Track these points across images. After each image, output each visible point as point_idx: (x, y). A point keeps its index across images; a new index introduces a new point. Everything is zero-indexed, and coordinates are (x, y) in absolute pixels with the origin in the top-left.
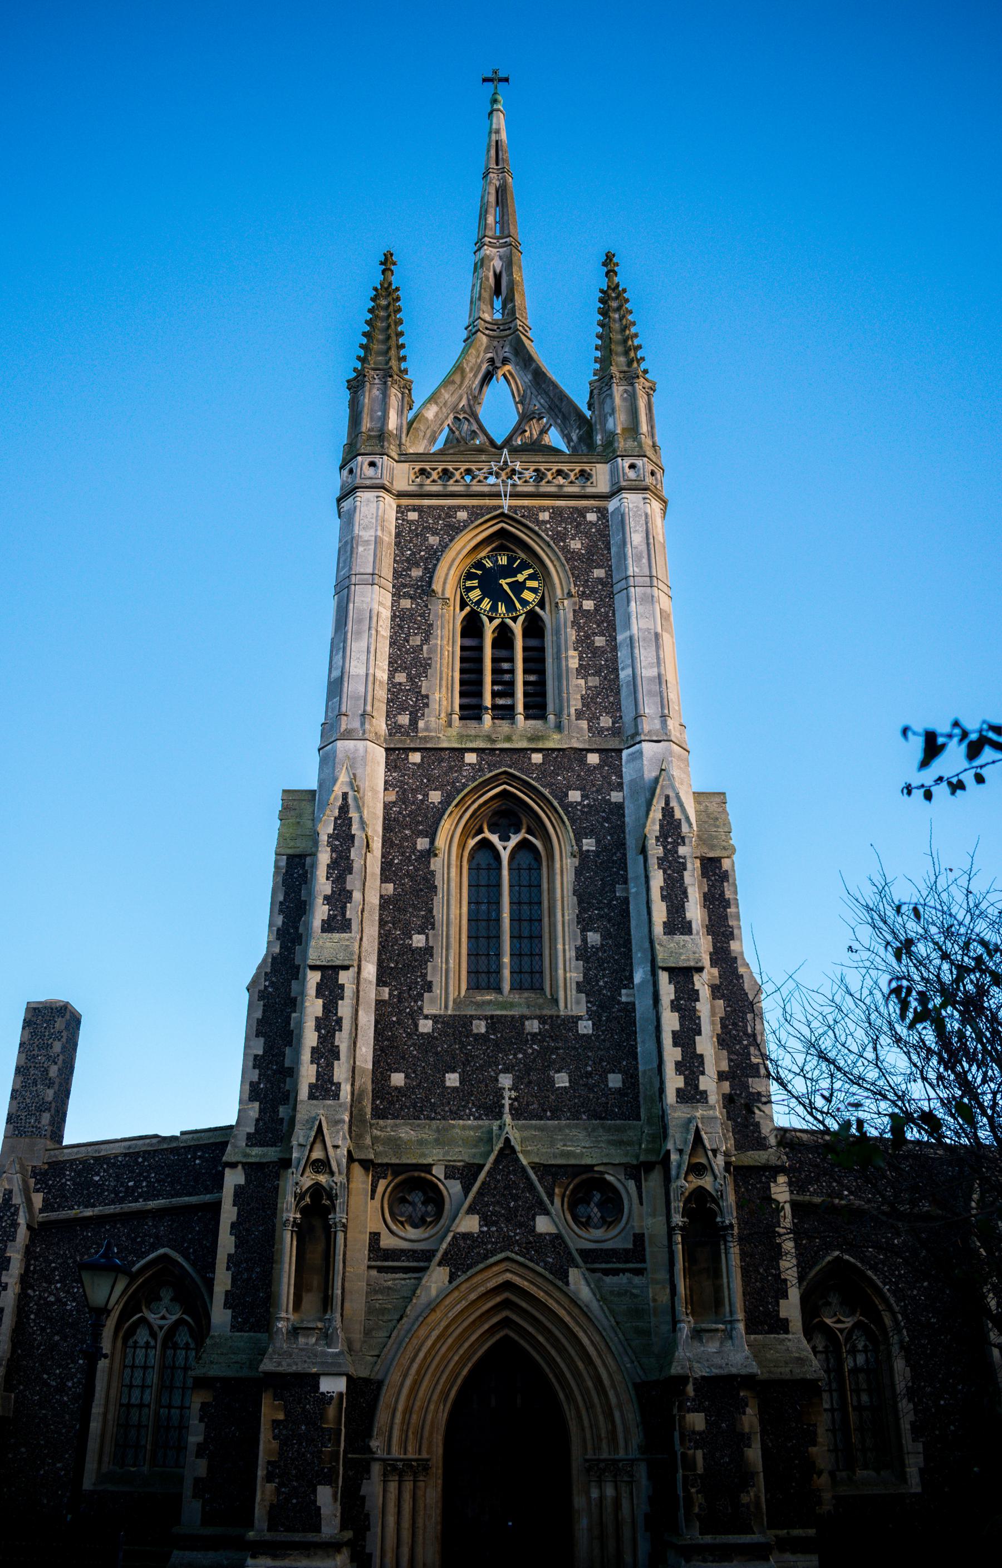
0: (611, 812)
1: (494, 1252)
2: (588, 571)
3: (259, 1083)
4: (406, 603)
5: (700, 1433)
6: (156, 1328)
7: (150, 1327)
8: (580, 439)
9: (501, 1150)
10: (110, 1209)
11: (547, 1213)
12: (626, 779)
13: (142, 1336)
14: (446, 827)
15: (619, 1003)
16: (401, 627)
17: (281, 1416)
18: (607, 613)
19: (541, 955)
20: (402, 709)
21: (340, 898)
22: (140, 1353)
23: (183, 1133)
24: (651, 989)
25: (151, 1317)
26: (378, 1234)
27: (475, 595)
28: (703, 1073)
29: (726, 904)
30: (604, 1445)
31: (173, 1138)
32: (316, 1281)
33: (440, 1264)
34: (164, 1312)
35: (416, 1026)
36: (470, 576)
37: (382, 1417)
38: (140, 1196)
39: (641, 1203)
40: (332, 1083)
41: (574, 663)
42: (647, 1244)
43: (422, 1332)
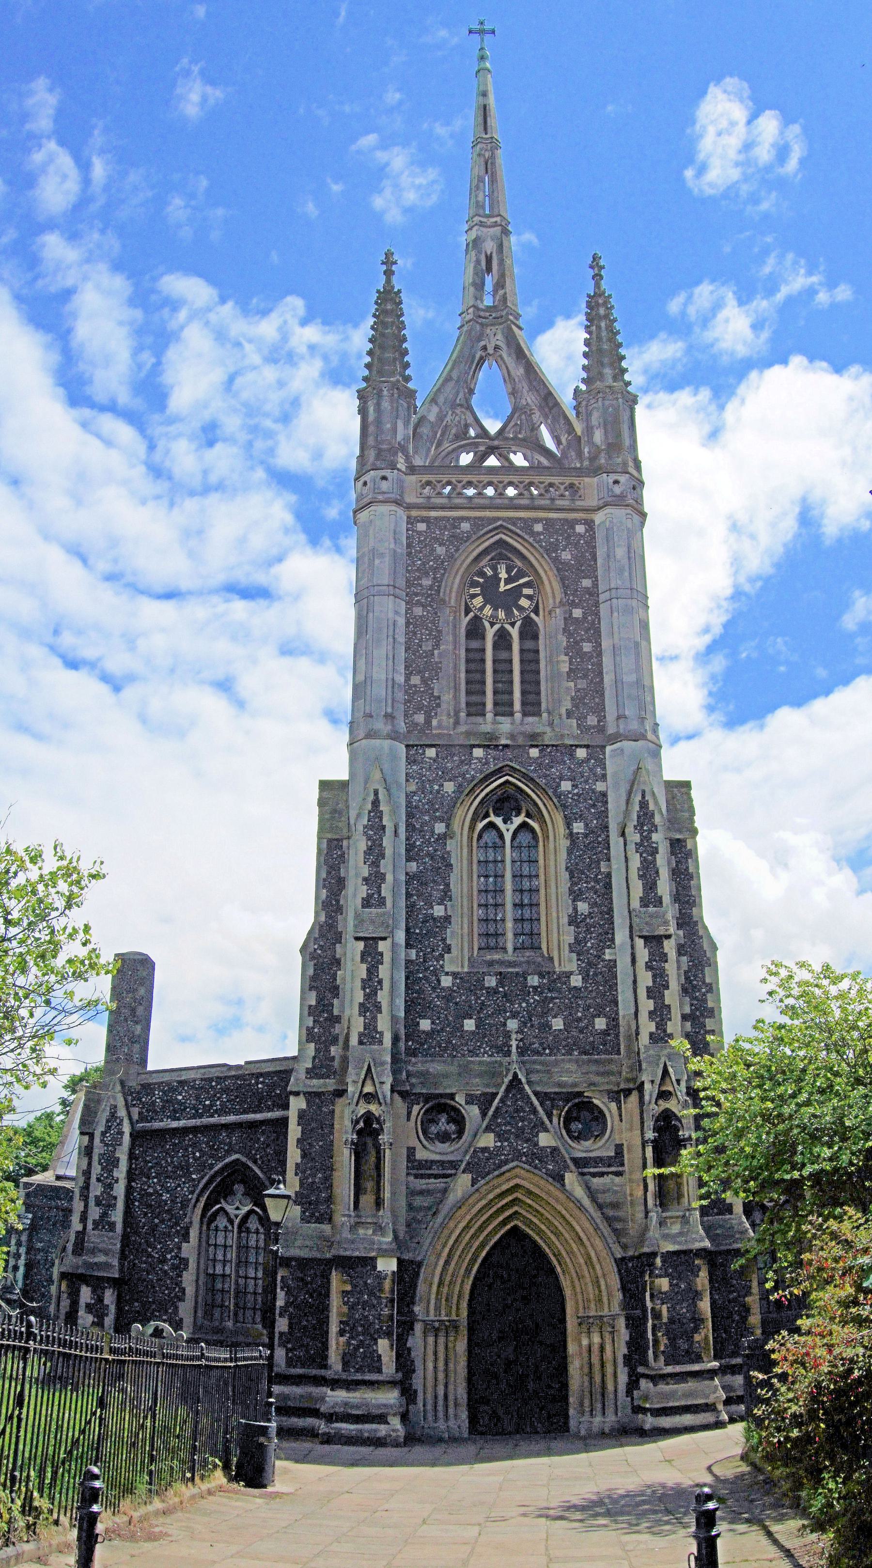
0: (597, 800)
1: (506, 1162)
2: (577, 581)
3: (313, 1028)
4: (418, 611)
5: (665, 1293)
6: (232, 1217)
7: (227, 1213)
8: (569, 443)
9: (511, 1082)
10: (192, 1122)
11: (546, 1130)
12: (609, 771)
13: (222, 1222)
14: (460, 813)
15: (604, 960)
16: (415, 634)
17: (348, 1288)
18: (593, 621)
19: (538, 920)
20: (419, 709)
21: (375, 880)
22: (221, 1234)
23: (247, 1063)
24: (629, 951)
25: (229, 1208)
26: (414, 1148)
27: (478, 601)
28: (670, 1019)
29: (690, 877)
30: (593, 1306)
31: (239, 1067)
32: (369, 1185)
33: (464, 1172)
34: (237, 1204)
35: (439, 981)
36: (474, 584)
37: (421, 1287)
38: (216, 1111)
39: (621, 1120)
40: (377, 1032)
41: (565, 668)
42: (625, 1152)
43: (452, 1224)
